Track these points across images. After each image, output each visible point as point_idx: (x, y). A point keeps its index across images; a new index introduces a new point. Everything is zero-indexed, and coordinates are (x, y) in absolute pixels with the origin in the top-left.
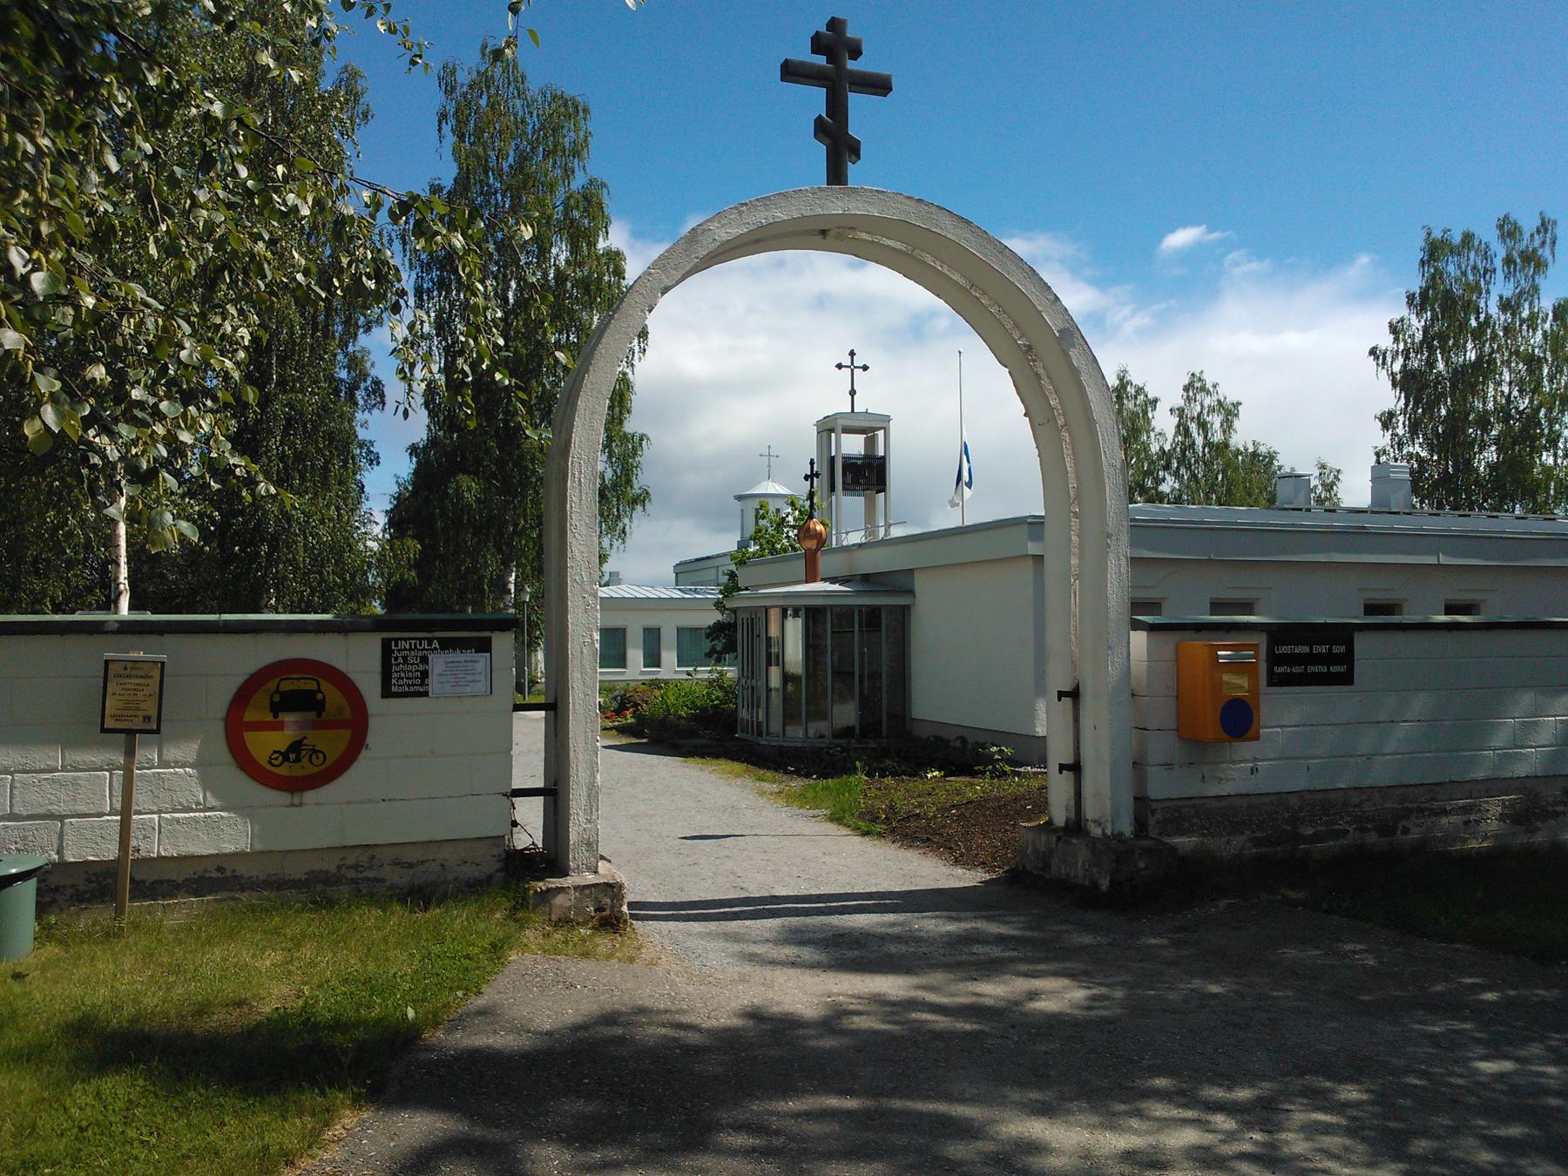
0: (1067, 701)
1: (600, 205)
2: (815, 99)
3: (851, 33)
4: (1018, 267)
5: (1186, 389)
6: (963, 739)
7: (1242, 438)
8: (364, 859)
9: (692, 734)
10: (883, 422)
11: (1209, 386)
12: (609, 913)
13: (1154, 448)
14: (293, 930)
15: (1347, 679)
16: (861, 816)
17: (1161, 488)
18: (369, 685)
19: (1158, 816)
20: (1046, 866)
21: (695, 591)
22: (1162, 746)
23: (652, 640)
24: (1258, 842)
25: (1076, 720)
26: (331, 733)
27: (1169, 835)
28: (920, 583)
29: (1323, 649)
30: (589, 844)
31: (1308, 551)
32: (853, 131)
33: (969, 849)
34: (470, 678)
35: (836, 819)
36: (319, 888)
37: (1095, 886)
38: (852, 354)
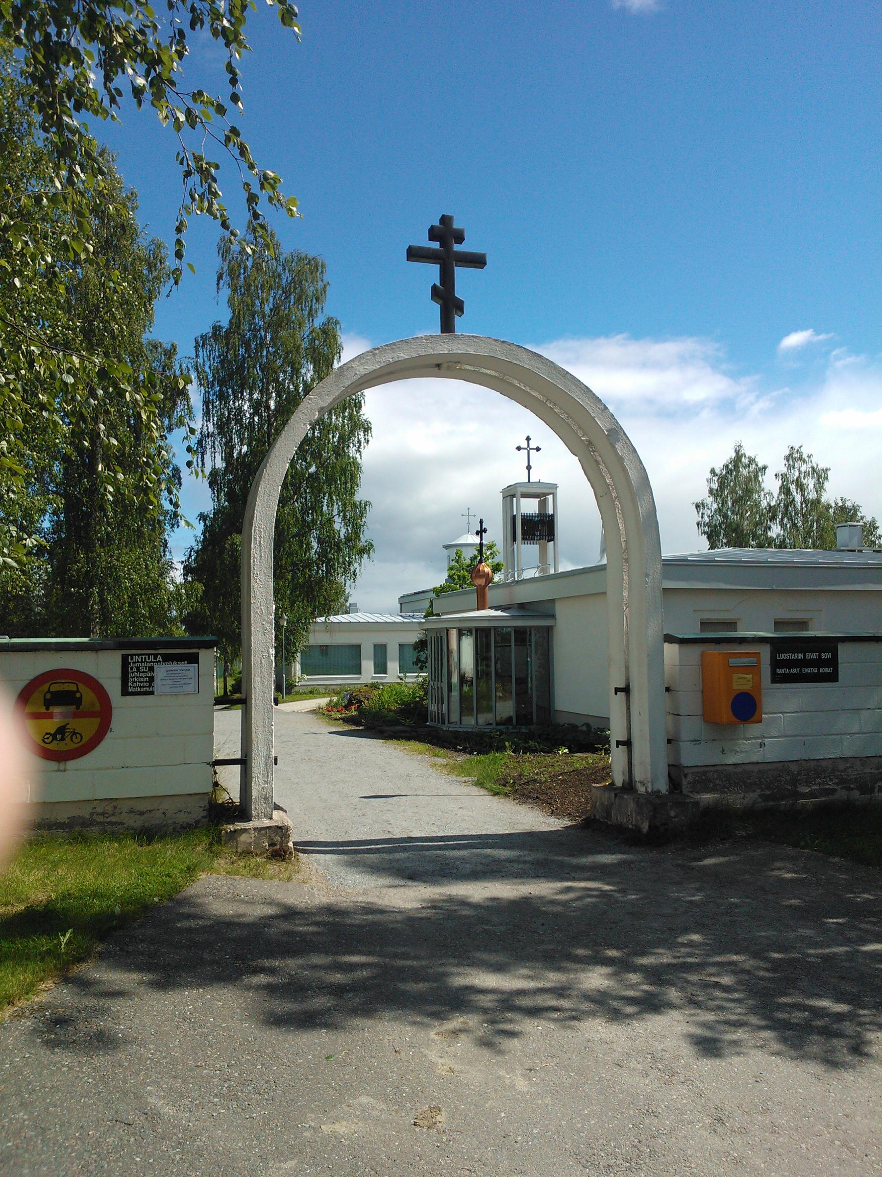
0: (621, 695)
1: (334, 337)
2: (431, 273)
3: (456, 225)
4: (576, 385)
5: (787, 458)
6: (588, 725)
7: (831, 495)
8: (109, 809)
9: (396, 723)
10: (552, 489)
11: (805, 456)
12: (279, 848)
13: (764, 504)
14: (56, 856)
15: (833, 677)
16: (496, 781)
17: (769, 534)
18: (113, 687)
19: (690, 778)
20: (609, 815)
21: (413, 617)
22: (691, 727)
23: (380, 652)
24: (766, 798)
25: (628, 708)
26: (85, 721)
27: (698, 792)
28: (561, 610)
29: (814, 656)
30: (266, 798)
31: (847, 583)
32: (458, 294)
33: (562, 804)
34: (183, 681)
35: (480, 784)
36: (77, 829)
37: (638, 830)
38: (528, 439)
